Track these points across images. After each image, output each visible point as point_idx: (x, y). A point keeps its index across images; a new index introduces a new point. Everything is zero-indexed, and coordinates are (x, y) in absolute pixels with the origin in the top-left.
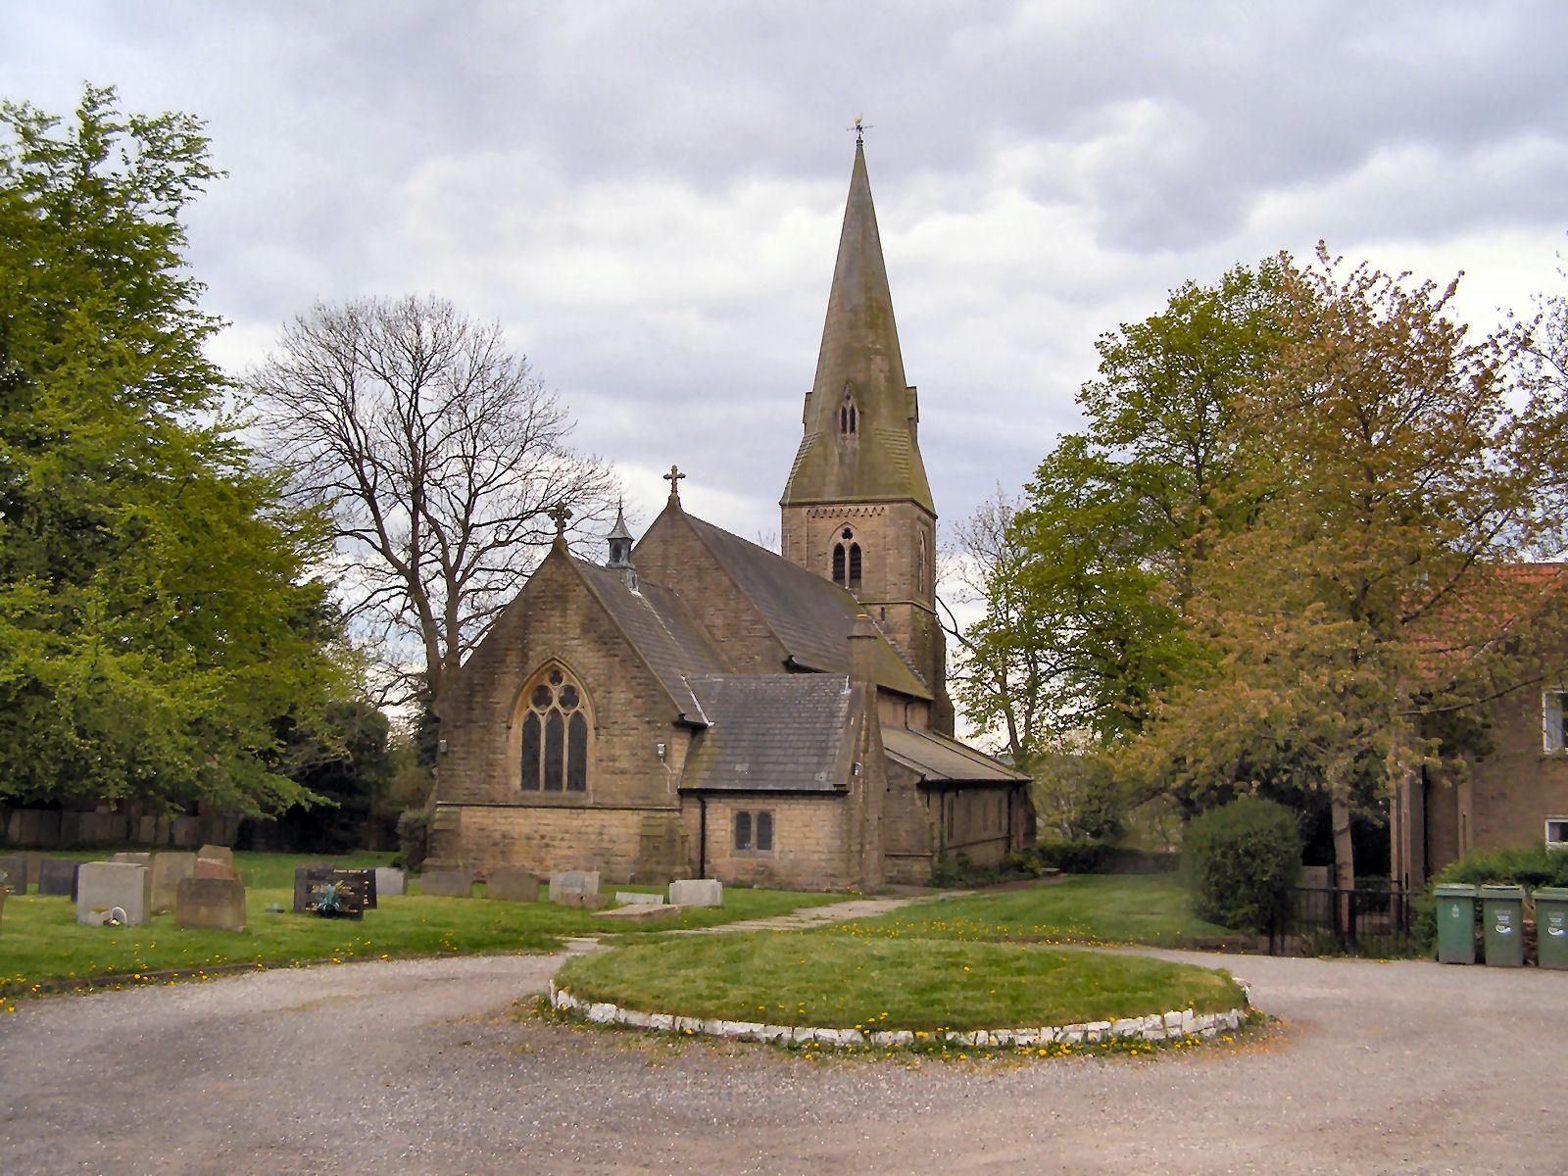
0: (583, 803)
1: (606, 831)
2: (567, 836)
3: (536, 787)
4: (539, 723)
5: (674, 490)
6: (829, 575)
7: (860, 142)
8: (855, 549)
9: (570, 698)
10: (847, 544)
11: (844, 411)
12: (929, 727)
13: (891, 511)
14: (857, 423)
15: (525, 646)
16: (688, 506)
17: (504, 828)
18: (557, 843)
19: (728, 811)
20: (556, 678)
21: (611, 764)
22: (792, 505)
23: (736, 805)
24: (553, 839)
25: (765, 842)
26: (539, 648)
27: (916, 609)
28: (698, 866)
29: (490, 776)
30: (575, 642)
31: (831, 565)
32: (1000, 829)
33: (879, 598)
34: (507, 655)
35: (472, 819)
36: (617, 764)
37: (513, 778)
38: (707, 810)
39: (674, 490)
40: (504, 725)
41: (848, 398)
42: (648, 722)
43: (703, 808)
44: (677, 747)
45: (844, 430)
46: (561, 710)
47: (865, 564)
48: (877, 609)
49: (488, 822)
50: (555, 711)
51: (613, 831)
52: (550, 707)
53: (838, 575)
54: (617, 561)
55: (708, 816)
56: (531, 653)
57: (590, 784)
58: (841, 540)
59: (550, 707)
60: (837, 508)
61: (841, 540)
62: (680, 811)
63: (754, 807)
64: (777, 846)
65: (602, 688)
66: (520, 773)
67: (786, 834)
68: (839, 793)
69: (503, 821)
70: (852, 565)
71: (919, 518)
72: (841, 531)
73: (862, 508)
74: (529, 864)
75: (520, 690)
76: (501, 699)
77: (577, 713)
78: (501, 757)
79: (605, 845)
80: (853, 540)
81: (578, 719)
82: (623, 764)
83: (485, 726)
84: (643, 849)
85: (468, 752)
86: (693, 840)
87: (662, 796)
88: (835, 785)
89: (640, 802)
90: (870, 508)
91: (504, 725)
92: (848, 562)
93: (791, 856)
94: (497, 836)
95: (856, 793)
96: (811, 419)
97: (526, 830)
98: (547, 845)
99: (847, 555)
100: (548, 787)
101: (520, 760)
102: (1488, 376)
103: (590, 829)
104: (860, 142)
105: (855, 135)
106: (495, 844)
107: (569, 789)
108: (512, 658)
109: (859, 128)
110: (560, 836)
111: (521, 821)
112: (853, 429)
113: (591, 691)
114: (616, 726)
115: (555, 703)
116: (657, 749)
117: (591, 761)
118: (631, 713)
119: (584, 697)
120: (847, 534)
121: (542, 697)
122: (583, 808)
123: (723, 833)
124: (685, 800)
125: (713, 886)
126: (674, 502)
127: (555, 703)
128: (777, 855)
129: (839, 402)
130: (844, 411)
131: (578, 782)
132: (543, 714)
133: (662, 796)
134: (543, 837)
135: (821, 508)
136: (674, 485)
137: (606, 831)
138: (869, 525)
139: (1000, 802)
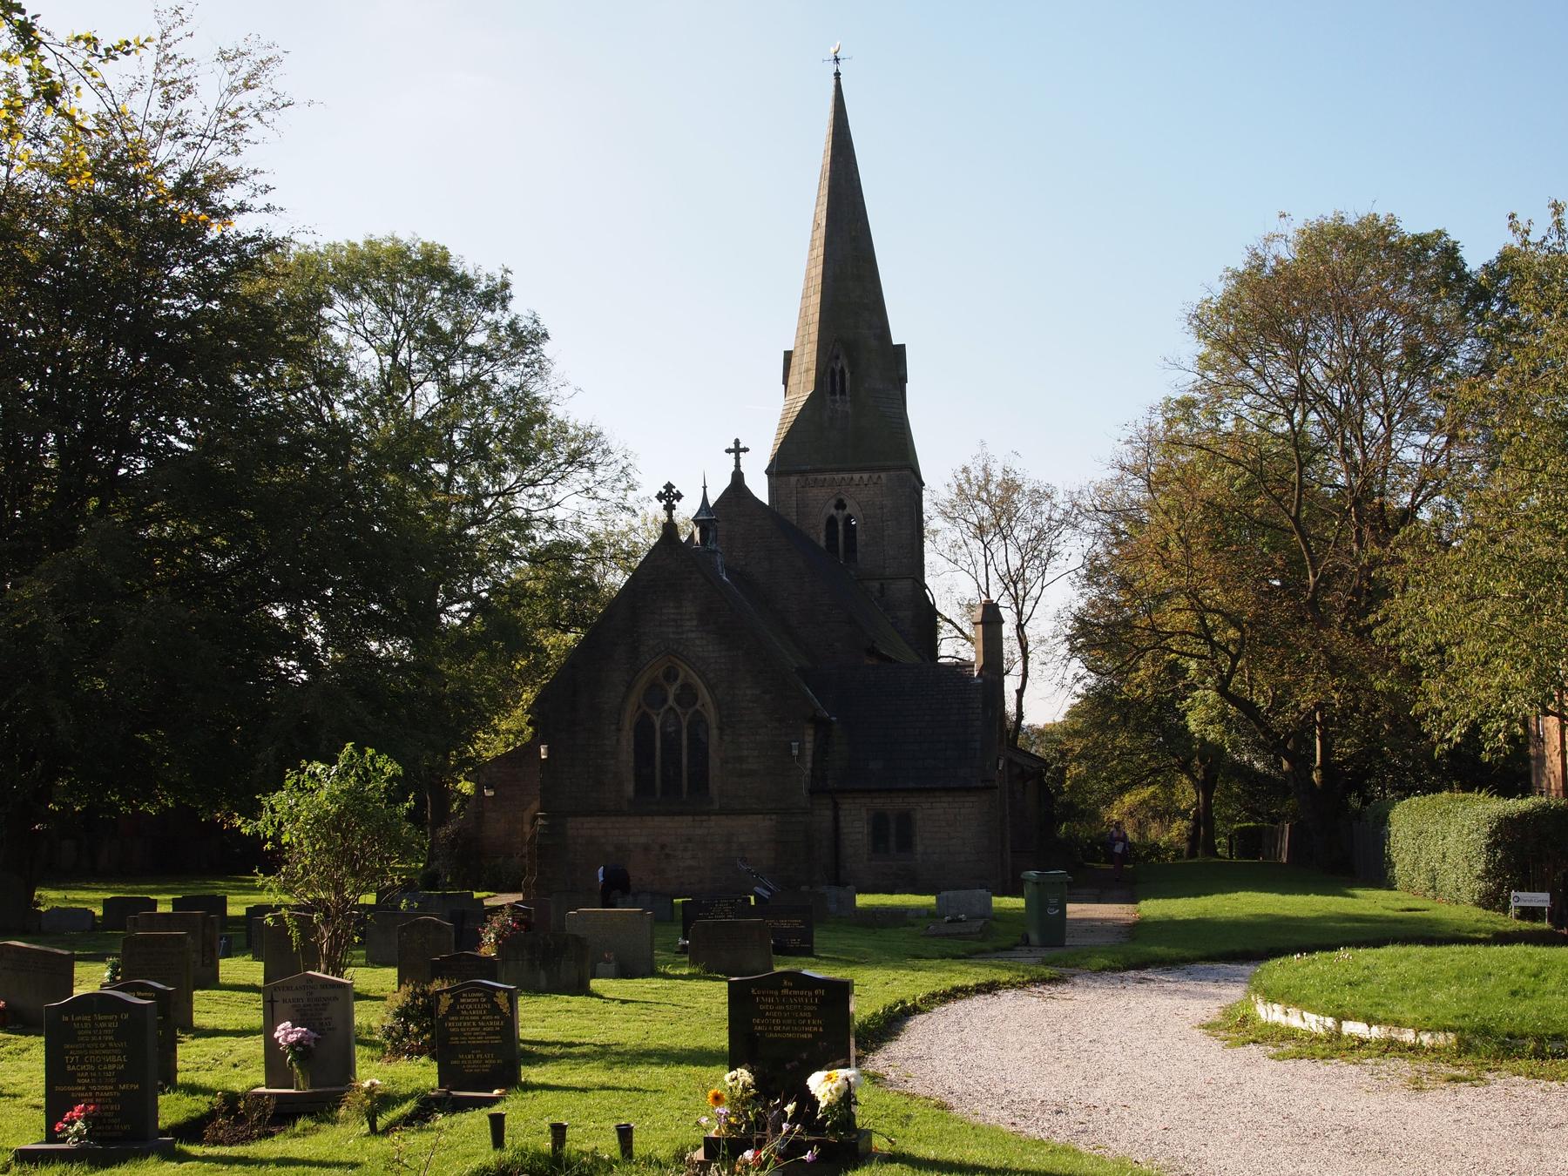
4: (652, 725)
5: (738, 465)
6: (822, 543)
7: (837, 75)
8: (850, 531)
9: (688, 696)
10: (840, 515)
11: (833, 370)
20: (670, 675)
25: (906, 843)
30: (693, 635)
39: (738, 465)
40: (613, 727)
41: (837, 358)
43: (836, 808)
45: (833, 392)
48: (877, 585)
52: (666, 707)
58: (833, 511)
59: (666, 707)
61: (833, 511)
64: (920, 849)
70: (845, 537)
72: (833, 502)
73: (856, 476)
81: (698, 721)
90: (866, 476)
91: (613, 727)
98: (668, 856)
101: (632, 764)
104: (837, 75)
105: (832, 68)
112: (843, 392)
113: (711, 688)
115: (671, 701)
117: (714, 762)
119: (704, 694)
120: (840, 505)
123: (860, 836)
127: (671, 701)
130: (833, 370)
131: (700, 780)
134: (663, 847)
135: (811, 477)
136: (737, 459)
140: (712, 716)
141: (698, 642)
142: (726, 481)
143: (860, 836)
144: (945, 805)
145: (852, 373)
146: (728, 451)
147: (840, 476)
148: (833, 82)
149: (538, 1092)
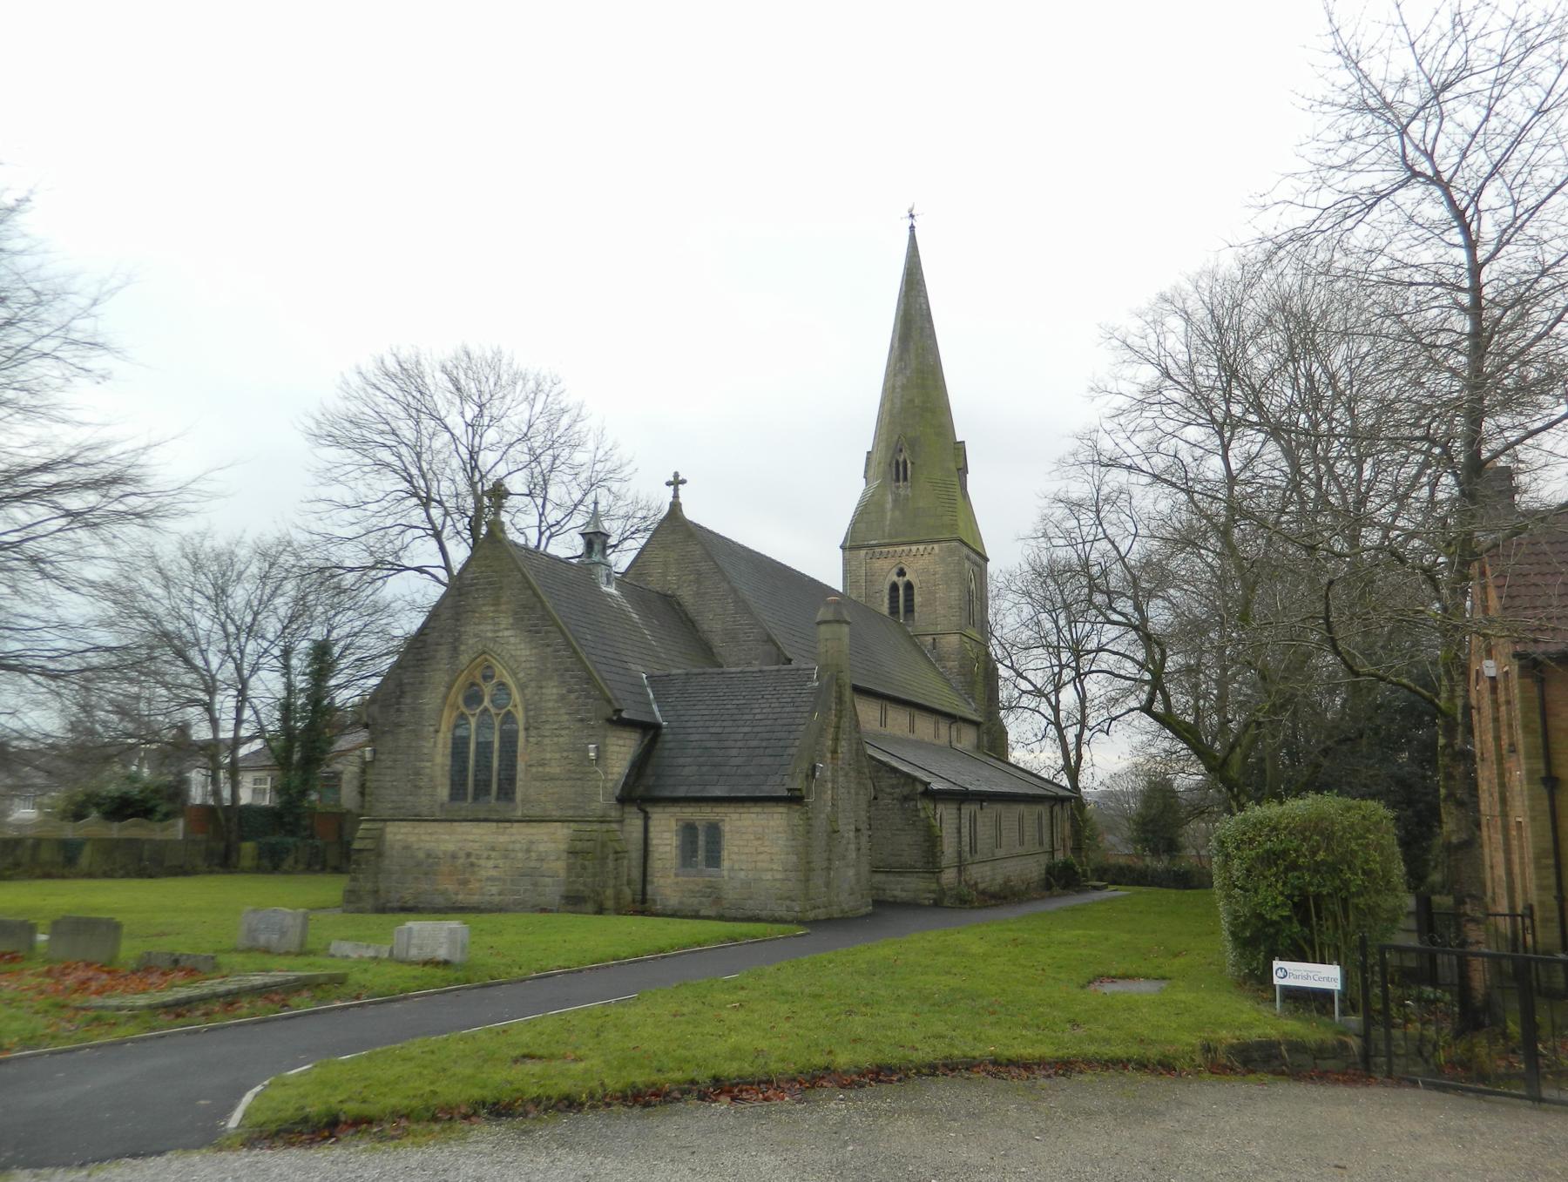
1: (534, 847)
2: (493, 854)
3: (464, 798)
5: (676, 496)
6: (885, 609)
7: (912, 228)
8: (909, 586)
10: (901, 581)
11: (897, 463)
12: (978, 747)
13: (941, 550)
14: (909, 473)
15: (456, 640)
16: (691, 513)
17: (428, 846)
18: (482, 862)
19: (673, 823)
21: (540, 769)
22: (852, 548)
23: (680, 816)
24: (478, 857)
25: (714, 859)
26: (470, 642)
27: (965, 639)
28: (639, 887)
29: (416, 786)
30: (507, 633)
31: (886, 601)
32: (1041, 843)
33: (931, 629)
34: (436, 651)
35: (398, 834)
36: (548, 769)
37: (439, 789)
38: (651, 823)
39: (676, 496)
40: (432, 729)
42: (582, 720)
43: (646, 818)
44: (616, 749)
45: (898, 480)
46: (493, 711)
47: (917, 599)
48: (929, 639)
49: (413, 839)
50: (486, 710)
51: (542, 848)
52: (481, 708)
53: (894, 610)
54: (590, 557)
55: (652, 829)
56: (463, 648)
57: (519, 796)
58: (895, 578)
59: (481, 708)
60: (891, 549)
61: (895, 578)
62: (621, 822)
63: (701, 815)
64: (726, 864)
65: (533, 684)
66: (447, 782)
67: (736, 849)
68: (794, 799)
69: (427, 838)
71: (968, 558)
72: (895, 570)
73: (914, 548)
74: (451, 887)
75: (450, 687)
76: (431, 699)
77: (509, 712)
78: (428, 764)
79: (533, 864)
80: (907, 577)
81: (509, 718)
82: (555, 770)
83: (414, 731)
84: (570, 868)
85: (395, 761)
86: (635, 855)
87: (594, 805)
88: (789, 790)
89: (571, 812)
90: (921, 547)
91: (432, 729)
92: (903, 598)
93: (742, 875)
94: (421, 855)
95: (823, 800)
96: (871, 473)
97: (451, 847)
98: (472, 865)
99: (901, 592)
100: (476, 798)
102: (1248, 877)
103: (518, 846)
104: (912, 228)
105: (908, 222)
106: (419, 864)
107: (498, 799)
108: (443, 653)
109: (912, 216)
110: (485, 854)
111: (447, 837)
112: (905, 479)
113: (522, 687)
114: (548, 727)
116: (588, 751)
118: (563, 711)
120: (901, 573)
121: (473, 698)
123: (668, 848)
124: (627, 809)
125: (452, 931)
126: (675, 506)
127: (486, 702)
128: (725, 873)
129: (893, 457)
130: (897, 463)
131: (507, 790)
132: (473, 715)
133: (594, 805)
134: (468, 855)
135: (878, 550)
136: (676, 491)
137: (534, 847)
138: (921, 563)
139: (1040, 817)
140: (520, 715)
141: (512, 640)
142: (666, 509)
143: (668, 848)
144: (753, 816)
145: (913, 463)
146: (668, 484)
147: (901, 548)
148: (907, 233)
149: (613, 1084)
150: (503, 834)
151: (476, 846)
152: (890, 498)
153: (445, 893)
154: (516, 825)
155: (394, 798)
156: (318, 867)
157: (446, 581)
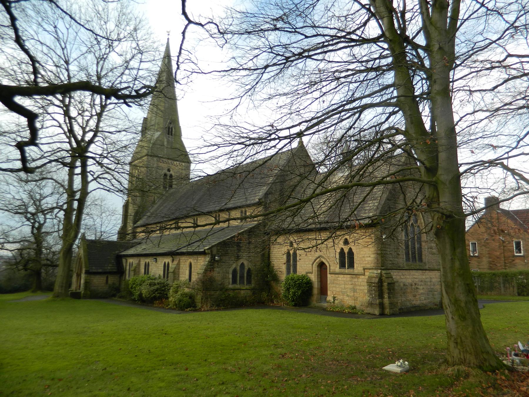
0: (425, 268)
7: (168, 39)
10: (168, 173)
11: (169, 128)
79: (432, 287)
80: (171, 172)
82: (434, 251)
97: (410, 281)
98: (417, 288)
104: (168, 39)
112: (172, 135)
122: (426, 270)
130: (169, 128)
150: (423, 275)
151: (417, 280)
152: (166, 140)
153: (410, 301)
154: (427, 271)
155: (391, 259)
156: (525, 293)
157: (63, 113)
